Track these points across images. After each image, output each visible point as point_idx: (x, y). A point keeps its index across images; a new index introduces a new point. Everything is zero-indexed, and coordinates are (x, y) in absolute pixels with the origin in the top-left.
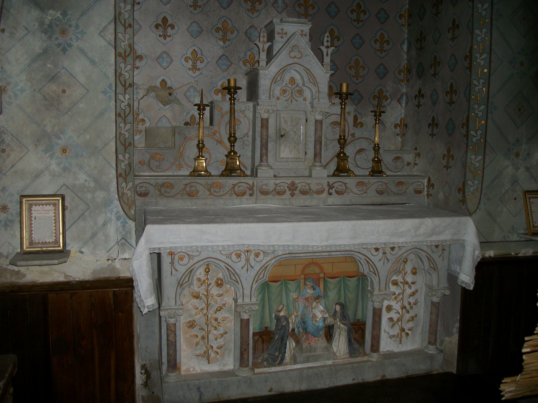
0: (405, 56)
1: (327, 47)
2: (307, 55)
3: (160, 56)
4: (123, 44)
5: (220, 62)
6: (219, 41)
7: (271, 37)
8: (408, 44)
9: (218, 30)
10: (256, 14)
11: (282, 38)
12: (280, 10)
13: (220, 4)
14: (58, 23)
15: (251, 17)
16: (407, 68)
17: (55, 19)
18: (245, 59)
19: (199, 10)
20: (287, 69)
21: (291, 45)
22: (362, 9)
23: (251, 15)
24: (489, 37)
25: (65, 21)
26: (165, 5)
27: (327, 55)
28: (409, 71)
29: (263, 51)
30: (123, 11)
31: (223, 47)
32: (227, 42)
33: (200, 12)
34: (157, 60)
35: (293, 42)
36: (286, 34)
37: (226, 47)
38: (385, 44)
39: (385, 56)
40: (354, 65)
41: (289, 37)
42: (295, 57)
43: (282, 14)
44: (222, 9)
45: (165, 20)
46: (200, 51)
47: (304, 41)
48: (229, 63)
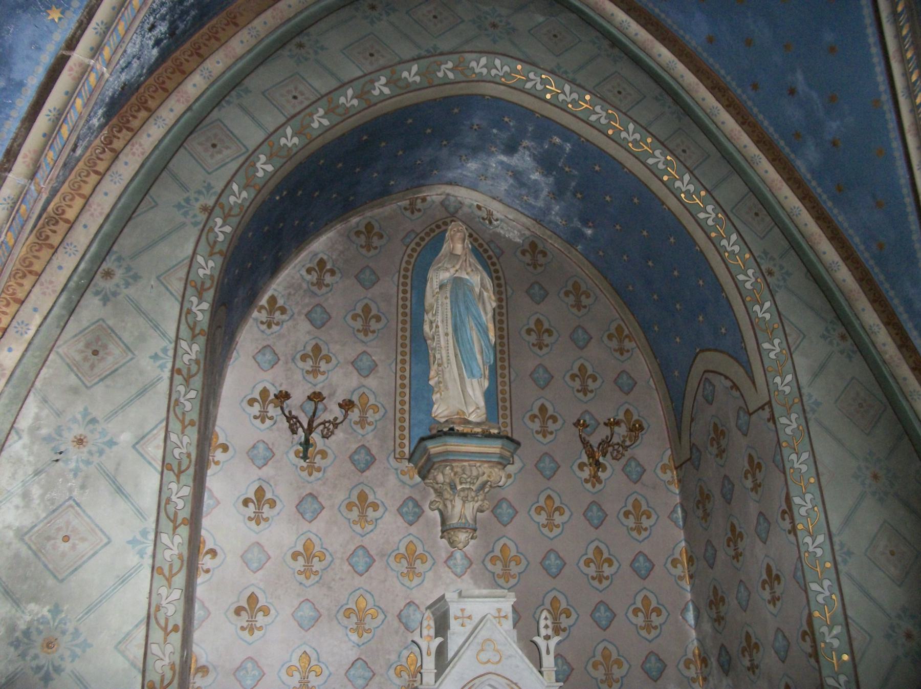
0: (693, 634)
1: (547, 638)
2: (510, 656)
3: (240, 666)
4: (159, 664)
5: (352, 672)
6: (349, 633)
7: (442, 627)
8: (694, 610)
9: (348, 613)
10: (416, 581)
11: (462, 625)
12: (459, 570)
13: (353, 567)
14: (41, 627)
15: (408, 587)
16: (700, 655)
17: (38, 620)
18: (399, 664)
19: (314, 579)
20: (476, 686)
21: (479, 639)
22: (604, 557)
23: (407, 583)
24: (838, 593)
25: (56, 624)
26: (255, 572)
27: (548, 652)
28: (704, 661)
29: (429, 654)
30: (164, 603)
31: (358, 645)
32: (365, 634)
33: (317, 582)
34: (234, 674)
35: (483, 634)
36: (470, 617)
37: (363, 644)
38: (654, 614)
39: (656, 637)
40: (602, 660)
41: (475, 624)
42: (488, 661)
43: (463, 577)
44: (355, 575)
45: (253, 599)
46: (315, 653)
47: (502, 631)
48: (368, 674)
